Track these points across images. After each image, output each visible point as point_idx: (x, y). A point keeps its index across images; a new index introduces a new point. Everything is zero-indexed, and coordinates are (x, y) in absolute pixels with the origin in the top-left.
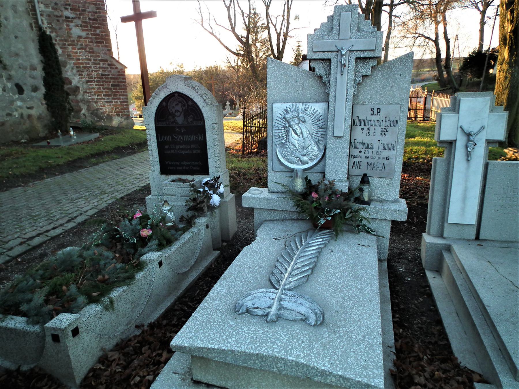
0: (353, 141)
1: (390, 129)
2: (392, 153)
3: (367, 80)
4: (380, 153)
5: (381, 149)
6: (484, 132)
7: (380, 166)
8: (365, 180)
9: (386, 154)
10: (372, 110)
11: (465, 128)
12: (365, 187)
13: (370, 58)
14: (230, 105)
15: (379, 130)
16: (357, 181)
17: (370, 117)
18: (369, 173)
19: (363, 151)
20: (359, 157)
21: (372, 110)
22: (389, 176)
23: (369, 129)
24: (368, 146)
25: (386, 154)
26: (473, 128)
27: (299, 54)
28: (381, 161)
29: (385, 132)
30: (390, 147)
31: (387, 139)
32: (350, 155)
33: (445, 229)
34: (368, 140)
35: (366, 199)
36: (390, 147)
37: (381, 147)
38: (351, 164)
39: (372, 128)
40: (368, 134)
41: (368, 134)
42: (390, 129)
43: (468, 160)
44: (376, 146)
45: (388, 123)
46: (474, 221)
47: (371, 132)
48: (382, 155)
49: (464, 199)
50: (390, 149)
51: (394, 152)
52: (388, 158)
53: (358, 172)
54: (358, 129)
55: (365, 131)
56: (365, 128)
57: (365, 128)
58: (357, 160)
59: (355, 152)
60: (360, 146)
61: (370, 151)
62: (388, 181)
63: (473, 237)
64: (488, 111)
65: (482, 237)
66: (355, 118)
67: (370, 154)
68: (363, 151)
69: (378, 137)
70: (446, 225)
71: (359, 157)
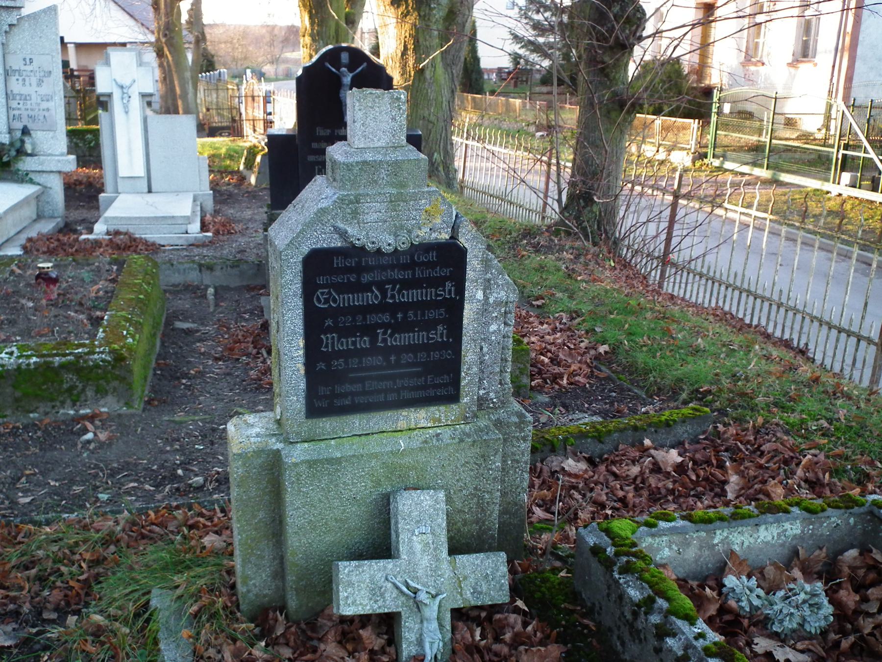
0: (9, 92)
1: (44, 79)
2: (51, 105)
3: (15, 30)
4: (39, 104)
5: (39, 101)
6: (135, 85)
7: (41, 118)
8: (25, 131)
9: (45, 105)
10: (24, 59)
11: (119, 81)
12: (26, 139)
13: (13, 8)
14: (414, 49)
15: (34, 80)
16: (18, 134)
17: (23, 68)
18: (30, 126)
19: (21, 102)
20: (19, 109)
21: (24, 59)
22: (52, 129)
23: (24, 80)
24: (25, 98)
25: (45, 105)
26: (126, 82)
27: (10, 633)
28: (42, 113)
29: (40, 82)
30: (48, 98)
31: (44, 90)
32: (8, 108)
33: (119, 184)
34: (25, 91)
35: (29, 152)
36: (48, 98)
37: (39, 98)
38: (11, 117)
39: (27, 79)
40: (24, 84)
41: (24, 84)
42: (44, 79)
43: (127, 113)
44: (34, 96)
45: (42, 74)
46: (141, 172)
47: (27, 83)
48: (42, 107)
49: (130, 151)
50: (48, 100)
51: (53, 103)
52: (48, 110)
53: (18, 125)
54: (13, 80)
55: (20, 82)
56: (21, 78)
57: (21, 78)
58: (16, 112)
59: (14, 104)
60: (18, 97)
61: (29, 102)
62: (51, 134)
63: (146, 190)
64: (135, 65)
65: (154, 189)
66: (8, 68)
67: (29, 107)
68: (21, 102)
69: (34, 87)
70: (119, 180)
71: (19, 109)
